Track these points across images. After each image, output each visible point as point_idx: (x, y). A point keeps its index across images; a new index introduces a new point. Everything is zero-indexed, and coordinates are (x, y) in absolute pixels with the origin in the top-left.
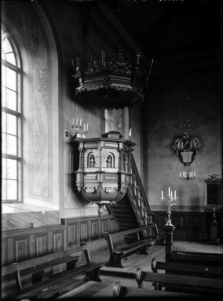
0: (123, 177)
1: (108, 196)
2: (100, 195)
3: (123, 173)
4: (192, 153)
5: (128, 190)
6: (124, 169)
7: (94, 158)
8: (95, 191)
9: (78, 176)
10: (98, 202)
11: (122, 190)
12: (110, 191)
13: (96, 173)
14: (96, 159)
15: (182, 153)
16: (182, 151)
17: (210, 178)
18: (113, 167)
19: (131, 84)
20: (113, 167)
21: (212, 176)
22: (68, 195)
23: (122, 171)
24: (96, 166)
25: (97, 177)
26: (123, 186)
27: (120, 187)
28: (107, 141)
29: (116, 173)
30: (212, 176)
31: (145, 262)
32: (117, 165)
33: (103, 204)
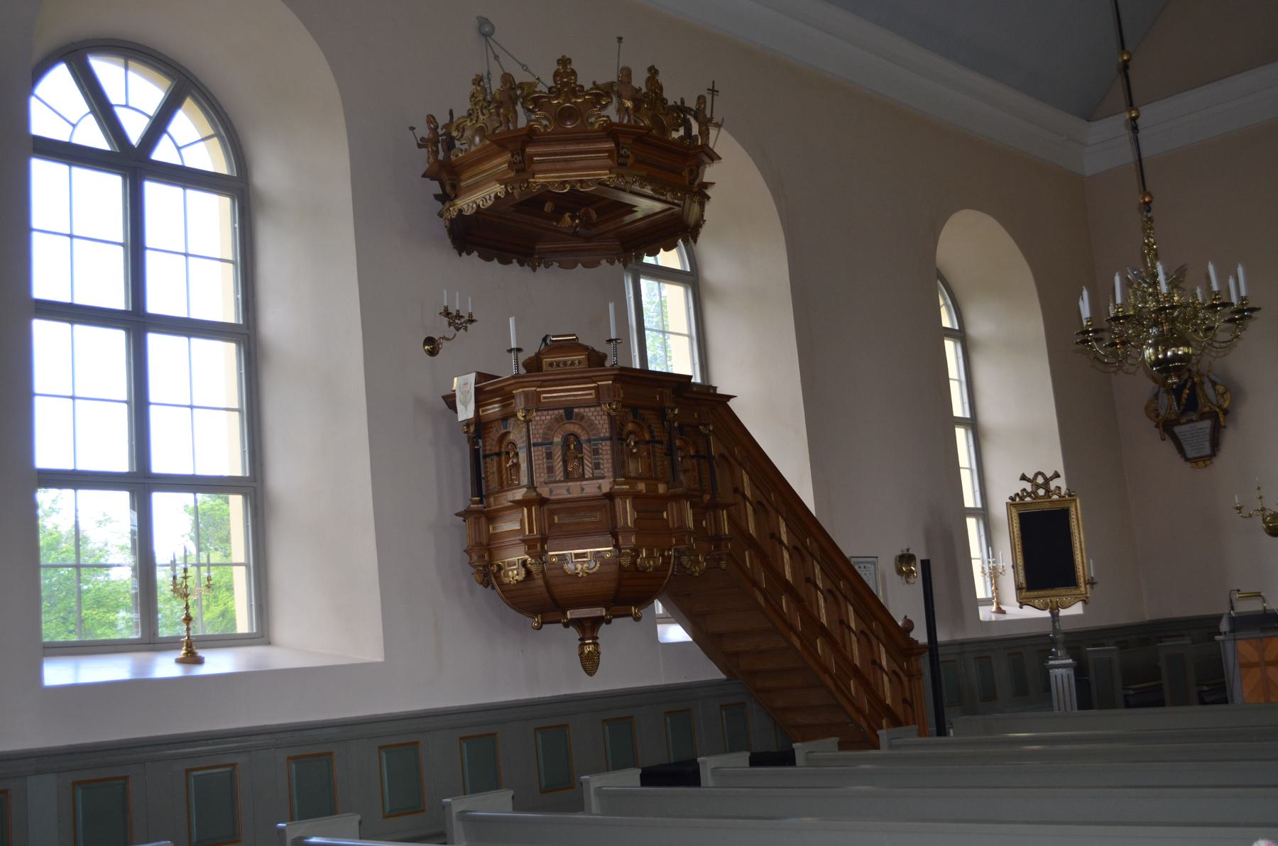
4: (1207, 424)
8: (528, 572)
15: (1177, 429)
16: (1177, 422)
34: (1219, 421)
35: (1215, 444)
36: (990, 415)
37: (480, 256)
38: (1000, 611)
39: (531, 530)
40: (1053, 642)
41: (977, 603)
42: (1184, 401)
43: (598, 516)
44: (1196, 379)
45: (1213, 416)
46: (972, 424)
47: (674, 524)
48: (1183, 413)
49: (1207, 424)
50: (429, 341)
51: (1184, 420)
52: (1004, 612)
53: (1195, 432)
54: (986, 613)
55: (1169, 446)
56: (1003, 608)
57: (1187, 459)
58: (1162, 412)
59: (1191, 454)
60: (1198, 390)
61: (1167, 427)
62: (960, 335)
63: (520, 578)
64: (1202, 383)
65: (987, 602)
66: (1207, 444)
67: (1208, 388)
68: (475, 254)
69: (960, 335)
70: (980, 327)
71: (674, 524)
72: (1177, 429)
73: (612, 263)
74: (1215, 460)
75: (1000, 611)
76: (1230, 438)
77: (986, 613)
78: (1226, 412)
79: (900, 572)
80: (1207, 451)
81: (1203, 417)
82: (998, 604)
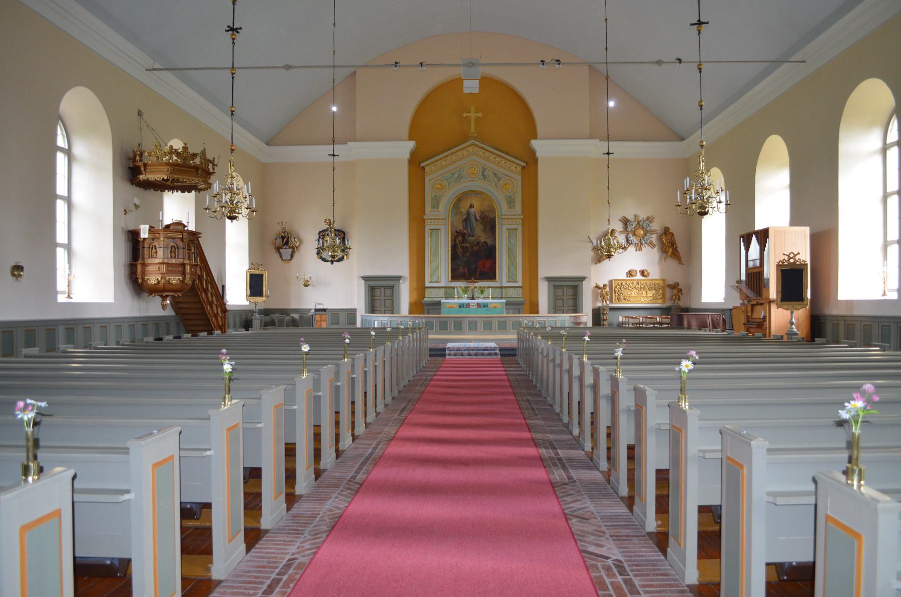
0: (188, 268)
1: (171, 287)
2: (660, 280)
3: (188, 264)
4: (290, 250)
5: (194, 281)
6: (189, 258)
7: (156, 249)
8: (158, 282)
9: (139, 268)
10: (161, 294)
11: (186, 281)
12: (174, 282)
13: (160, 263)
14: (158, 249)
15: (281, 250)
16: (282, 248)
17: (786, 258)
18: (177, 257)
19: (204, 184)
20: (177, 257)
21: (788, 256)
22: (126, 290)
23: (187, 262)
24: (158, 256)
25: (159, 268)
26: (188, 276)
27: (184, 278)
28: (170, 231)
29: (180, 264)
30: (788, 256)
31: (462, 351)
32: (181, 256)
33: (167, 296)
34: (294, 250)
35: (292, 256)
36: (76, 197)
37: (154, 190)
38: (69, 297)
39: (163, 271)
40: (255, 312)
41: (55, 293)
42: (284, 242)
43: (180, 269)
44: (289, 236)
45: (293, 248)
46: (68, 200)
47: (163, 267)
48: (284, 245)
49: (290, 250)
50: (125, 211)
51: (284, 248)
52: (71, 298)
53: (286, 252)
54: (62, 299)
55: (277, 255)
56: (71, 296)
57: (283, 260)
58: (277, 244)
59: (284, 259)
60: (289, 239)
61: (278, 249)
62: (68, 152)
63: (156, 282)
64: (291, 237)
65: (63, 293)
66: (290, 256)
67: (293, 239)
68: (152, 189)
69: (68, 152)
70: (79, 149)
71: (163, 267)
72: (281, 250)
73: (169, 191)
74: (291, 261)
75: (69, 297)
76: (296, 255)
77: (62, 299)
78: (297, 247)
79: (13, 275)
80: (289, 258)
81: (290, 248)
82: (68, 294)
